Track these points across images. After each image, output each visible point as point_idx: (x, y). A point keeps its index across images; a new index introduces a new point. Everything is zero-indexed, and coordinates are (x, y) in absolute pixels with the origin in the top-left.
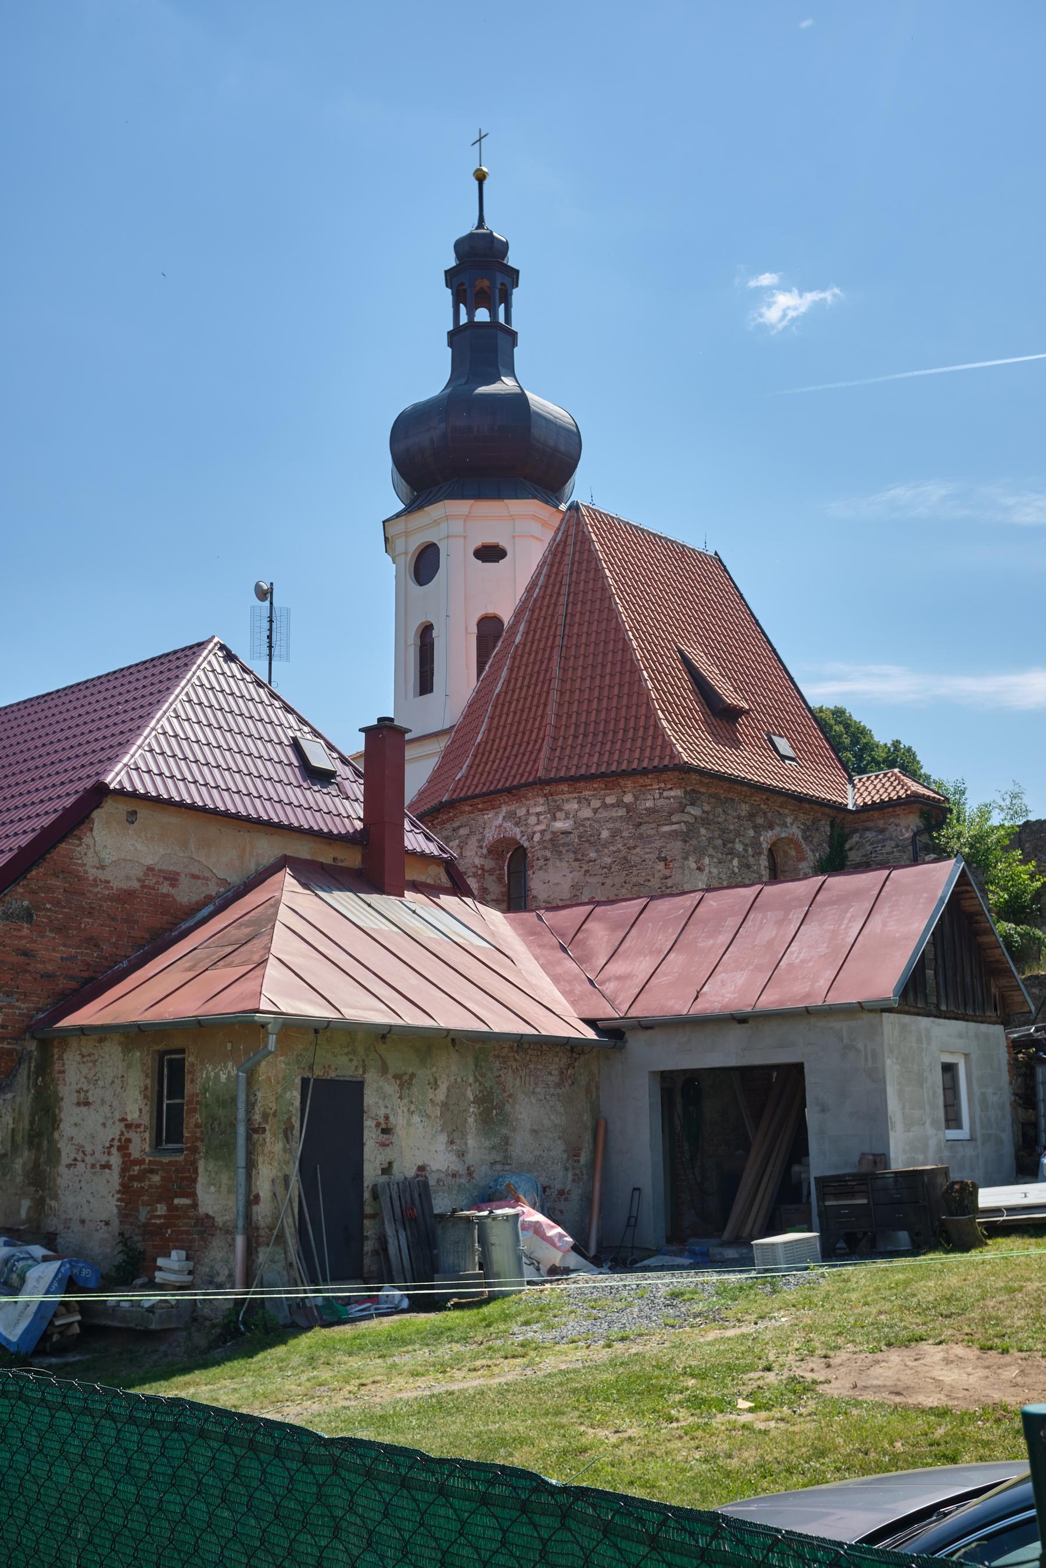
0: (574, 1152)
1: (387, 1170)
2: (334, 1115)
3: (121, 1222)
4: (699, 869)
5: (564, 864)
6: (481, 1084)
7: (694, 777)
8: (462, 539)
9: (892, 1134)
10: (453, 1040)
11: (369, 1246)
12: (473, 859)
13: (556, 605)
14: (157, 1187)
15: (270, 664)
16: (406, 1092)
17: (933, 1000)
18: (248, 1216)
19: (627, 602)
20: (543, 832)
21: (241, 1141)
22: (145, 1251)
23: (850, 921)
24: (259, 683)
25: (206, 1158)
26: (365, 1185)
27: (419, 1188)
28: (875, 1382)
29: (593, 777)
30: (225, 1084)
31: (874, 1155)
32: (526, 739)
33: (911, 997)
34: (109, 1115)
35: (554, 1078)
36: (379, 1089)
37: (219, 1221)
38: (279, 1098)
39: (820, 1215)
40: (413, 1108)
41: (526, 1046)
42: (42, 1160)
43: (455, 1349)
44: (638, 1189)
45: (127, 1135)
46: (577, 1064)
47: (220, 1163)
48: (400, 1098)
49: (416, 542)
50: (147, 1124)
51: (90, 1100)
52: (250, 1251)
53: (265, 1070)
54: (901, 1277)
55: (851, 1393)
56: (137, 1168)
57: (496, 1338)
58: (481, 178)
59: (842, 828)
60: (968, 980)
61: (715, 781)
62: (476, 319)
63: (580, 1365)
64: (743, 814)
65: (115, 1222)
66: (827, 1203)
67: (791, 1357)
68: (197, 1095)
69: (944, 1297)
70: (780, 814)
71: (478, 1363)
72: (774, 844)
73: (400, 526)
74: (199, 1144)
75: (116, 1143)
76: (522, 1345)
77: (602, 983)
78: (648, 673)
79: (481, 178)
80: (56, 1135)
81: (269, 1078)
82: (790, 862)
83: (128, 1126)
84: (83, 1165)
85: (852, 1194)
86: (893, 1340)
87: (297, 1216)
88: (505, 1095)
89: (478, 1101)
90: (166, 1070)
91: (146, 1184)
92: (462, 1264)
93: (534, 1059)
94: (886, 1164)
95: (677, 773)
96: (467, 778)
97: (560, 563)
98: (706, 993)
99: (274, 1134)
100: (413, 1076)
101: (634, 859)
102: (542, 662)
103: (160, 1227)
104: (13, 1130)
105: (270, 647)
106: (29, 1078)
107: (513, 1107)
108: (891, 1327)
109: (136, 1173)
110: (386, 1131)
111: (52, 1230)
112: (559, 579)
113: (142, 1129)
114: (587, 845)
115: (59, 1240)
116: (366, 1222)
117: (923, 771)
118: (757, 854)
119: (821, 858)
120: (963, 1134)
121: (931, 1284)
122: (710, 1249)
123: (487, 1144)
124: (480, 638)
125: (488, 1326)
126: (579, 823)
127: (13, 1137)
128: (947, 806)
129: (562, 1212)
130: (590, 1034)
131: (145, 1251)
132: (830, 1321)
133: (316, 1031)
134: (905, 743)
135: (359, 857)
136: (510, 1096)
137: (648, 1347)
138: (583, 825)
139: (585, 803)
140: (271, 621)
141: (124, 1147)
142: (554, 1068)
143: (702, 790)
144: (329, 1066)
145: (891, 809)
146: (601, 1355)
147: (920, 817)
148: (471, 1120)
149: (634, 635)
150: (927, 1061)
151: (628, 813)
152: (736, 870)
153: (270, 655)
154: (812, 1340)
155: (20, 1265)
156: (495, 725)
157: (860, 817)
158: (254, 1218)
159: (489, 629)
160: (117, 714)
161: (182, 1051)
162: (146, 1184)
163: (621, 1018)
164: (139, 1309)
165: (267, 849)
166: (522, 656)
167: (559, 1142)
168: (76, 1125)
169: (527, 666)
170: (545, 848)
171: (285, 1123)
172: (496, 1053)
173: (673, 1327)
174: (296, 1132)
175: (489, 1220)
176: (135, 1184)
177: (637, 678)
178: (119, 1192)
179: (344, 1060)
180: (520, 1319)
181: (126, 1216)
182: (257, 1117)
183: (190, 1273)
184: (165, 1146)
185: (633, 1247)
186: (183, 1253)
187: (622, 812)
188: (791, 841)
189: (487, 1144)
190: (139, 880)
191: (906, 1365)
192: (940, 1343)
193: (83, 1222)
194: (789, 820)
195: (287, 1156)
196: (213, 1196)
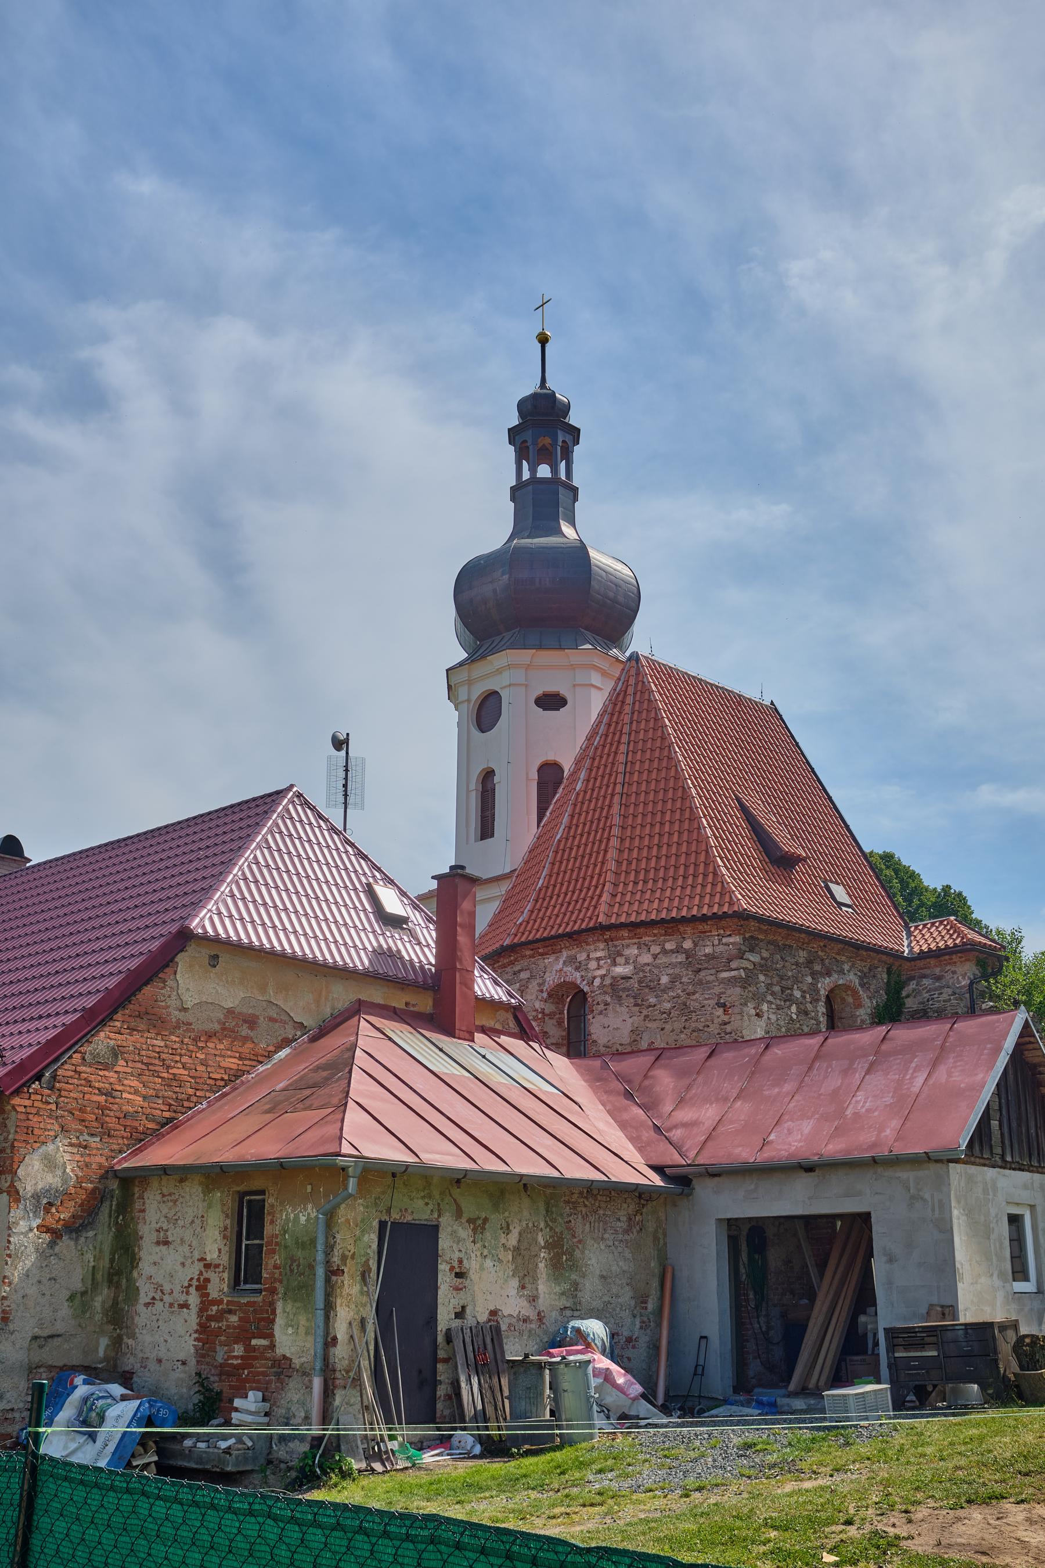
0: (641, 1300)
1: (460, 1315)
2: (409, 1258)
3: (198, 1362)
4: (757, 1015)
5: (624, 1009)
6: (551, 1229)
7: (753, 923)
8: (523, 689)
9: (960, 1285)
10: (525, 1185)
11: (442, 1391)
12: (534, 1002)
13: (616, 753)
14: (235, 1328)
15: (345, 812)
16: (479, 1236)
17: (998, 1150)
18: (326, 1359)
19: (686, 750)
20: (603, 977)
21: (320, 1283)
22: (221, 1391)
23: (914, 1071)
24: (333, 829)
25: (284, 1299)
26: (439, 1329)
27: (492, 1333)
28: (959, 1540)
29: (653, 923)
30: (305, 1226)
31: (942, 1307)
32: (586, 884)
33: (977, 1148)
34: (188, 1254)
35: (622, 1225)
36: (454, 1233)
37: (297, 1362)
38: (357, 1240)
39: (889, 1366)
40: (486, 1252)
41: (595, 1192)
42: (120, 1298)
43: (533, 1496)
44: (706, 1337)
45: (206, 1275)
46: (645, 1210)
47: (298, 1304)
48: (474, 1242)
49: (479, 690)
50: (226, 1264)
51: (170, 1239)
52: (328, 1393)
53: (344, 1214)
54: (974, 1431)
55: (936, 1550)
56: (215, 1308)
57: (573, 1486)
58: (543, 340)
59: (899, 976)
60: (1033, 1131)
61: (774, 928)
62: (539, 475)
63: (658, 1515)
64: (801, 960)
65: (192, 1362)
66: (897, 1355)
67: (871, 1511)
68: (277, 1236)
69: (1020, 1454)
70: (838, 961)
71: (557, 1510)
72: (831, 991)
73: (463, 675)
74: (277, 1285)
75: (195, 1283)
76: (600, 1494)
77: (669, 1130)
78: (707, 821)
79: (543, 340)
80: (135, 1274)
81: (348, 1221)
82: (848, 1009)
83: (207, 1266)
84: (161, 1304)
85: (922, 1345)
86: (973, 1497)
87: (372, 1359)
88: (575, 1240)
89: (548, 1246)
90: (245, 1210)
91: (223, 1324)
92: (534, 1411)
93: (603, 1205)
94: (955, 1316)
95: (736, 920)
96: (528, 923)
97: (620, 713)
98: (772, 1142)
99: (352, 1277)
100: (486, 1220)
101: (693, 1005)
102: (602, 809)
103: (236, 1367)
104: (94, 1267)
105: (346, 795)
106: (110, 1216)
107: (583, 1253)
108: (970, 1484)
109: (214, 1313)
110: (459, 1275)
111: (127, 1369)
112: (619, 728)
113: (221, 1269)
114: (647, 990)
115: (135, 1379)
116: (440, 1366)
117: (974, 916)
118: (815, 1001)
119: (878, 1005)
120: (1029, 1287)
121: (1007, 1440)
122: (778, 1400)
123: (557, 1289)
124: (541, 785)
125: (563, 1473)
126: (638, 969)
127: (93, 1274)
128: (1003, 954)
129: (629, 1359)
130: (657, 1180)
131: (221, 1391)
132: (908, 1475)
133: (394, 1175)
134: (956, 888)
135: (430, 1003)
136: (580, 1242)
137: (726, 1498)
138: (643, 971)
139: (644, 949)
140: (347, 771)
141: (202, 1287)
142: (622, 1214)
143: (761, 937)
144: (406, 1210)
145: (947, 957)
146: (681, 1505)
147: (977, 965)
148: (541, 1265)
149: (693, 783)
150: (993, 1212)
151: (687, 958)
152: (794, 1017)
153: (345, 803)
154: (890, 1494)
155: (100, 1403)
156: (555, 870)
157: (911, 967)
158: (331, 1361)
159: (549, 777)
160: (199, 859)
161: (262, 1192)
162: (223, 1324)
163: (689, 1165)
164: (216, 1450)
165: (342, 995)
166: (583, 803)
167: (627, 1288)
168: (155, 1263)
169: (587, 813)
170: (606, 993)
171: (363, 1266)
172: (566, 1198)
173: (749, 1477)
174: (373, 1275)
175: (562, 1366)
176: (213, 1324)
177: (696, 826)
178: (196, 1332)
179: (420, 1203)
180: (595, 1467)
181: (203, 1356)
182: (336, 1259)
183: (266, 1414)
184: (243, 1287)
185: (700, 1397)
186: (260, 1394)
187: (681, 958)
188: (847, 987)
189: (557, 1289)
190: (219, 1022)
191: (989, 1524)
192: (1022, 1501)
193: (160, 1361)
194: (846, 967)
195: (365, 1299)
196: (291, 1338)
